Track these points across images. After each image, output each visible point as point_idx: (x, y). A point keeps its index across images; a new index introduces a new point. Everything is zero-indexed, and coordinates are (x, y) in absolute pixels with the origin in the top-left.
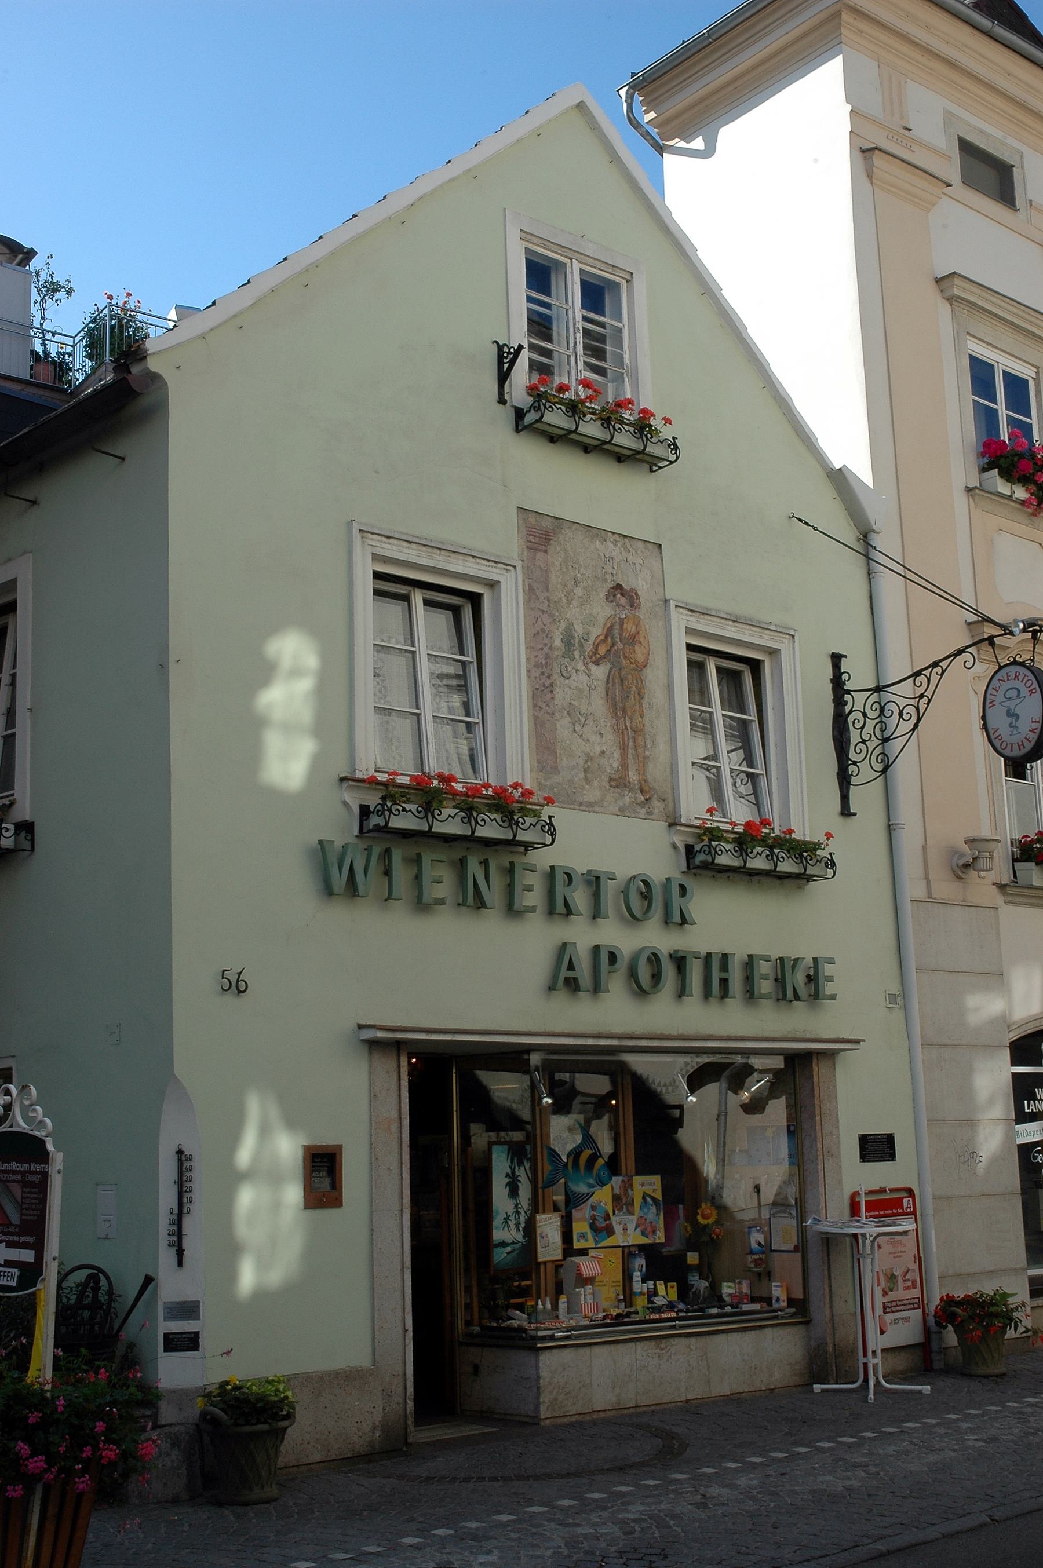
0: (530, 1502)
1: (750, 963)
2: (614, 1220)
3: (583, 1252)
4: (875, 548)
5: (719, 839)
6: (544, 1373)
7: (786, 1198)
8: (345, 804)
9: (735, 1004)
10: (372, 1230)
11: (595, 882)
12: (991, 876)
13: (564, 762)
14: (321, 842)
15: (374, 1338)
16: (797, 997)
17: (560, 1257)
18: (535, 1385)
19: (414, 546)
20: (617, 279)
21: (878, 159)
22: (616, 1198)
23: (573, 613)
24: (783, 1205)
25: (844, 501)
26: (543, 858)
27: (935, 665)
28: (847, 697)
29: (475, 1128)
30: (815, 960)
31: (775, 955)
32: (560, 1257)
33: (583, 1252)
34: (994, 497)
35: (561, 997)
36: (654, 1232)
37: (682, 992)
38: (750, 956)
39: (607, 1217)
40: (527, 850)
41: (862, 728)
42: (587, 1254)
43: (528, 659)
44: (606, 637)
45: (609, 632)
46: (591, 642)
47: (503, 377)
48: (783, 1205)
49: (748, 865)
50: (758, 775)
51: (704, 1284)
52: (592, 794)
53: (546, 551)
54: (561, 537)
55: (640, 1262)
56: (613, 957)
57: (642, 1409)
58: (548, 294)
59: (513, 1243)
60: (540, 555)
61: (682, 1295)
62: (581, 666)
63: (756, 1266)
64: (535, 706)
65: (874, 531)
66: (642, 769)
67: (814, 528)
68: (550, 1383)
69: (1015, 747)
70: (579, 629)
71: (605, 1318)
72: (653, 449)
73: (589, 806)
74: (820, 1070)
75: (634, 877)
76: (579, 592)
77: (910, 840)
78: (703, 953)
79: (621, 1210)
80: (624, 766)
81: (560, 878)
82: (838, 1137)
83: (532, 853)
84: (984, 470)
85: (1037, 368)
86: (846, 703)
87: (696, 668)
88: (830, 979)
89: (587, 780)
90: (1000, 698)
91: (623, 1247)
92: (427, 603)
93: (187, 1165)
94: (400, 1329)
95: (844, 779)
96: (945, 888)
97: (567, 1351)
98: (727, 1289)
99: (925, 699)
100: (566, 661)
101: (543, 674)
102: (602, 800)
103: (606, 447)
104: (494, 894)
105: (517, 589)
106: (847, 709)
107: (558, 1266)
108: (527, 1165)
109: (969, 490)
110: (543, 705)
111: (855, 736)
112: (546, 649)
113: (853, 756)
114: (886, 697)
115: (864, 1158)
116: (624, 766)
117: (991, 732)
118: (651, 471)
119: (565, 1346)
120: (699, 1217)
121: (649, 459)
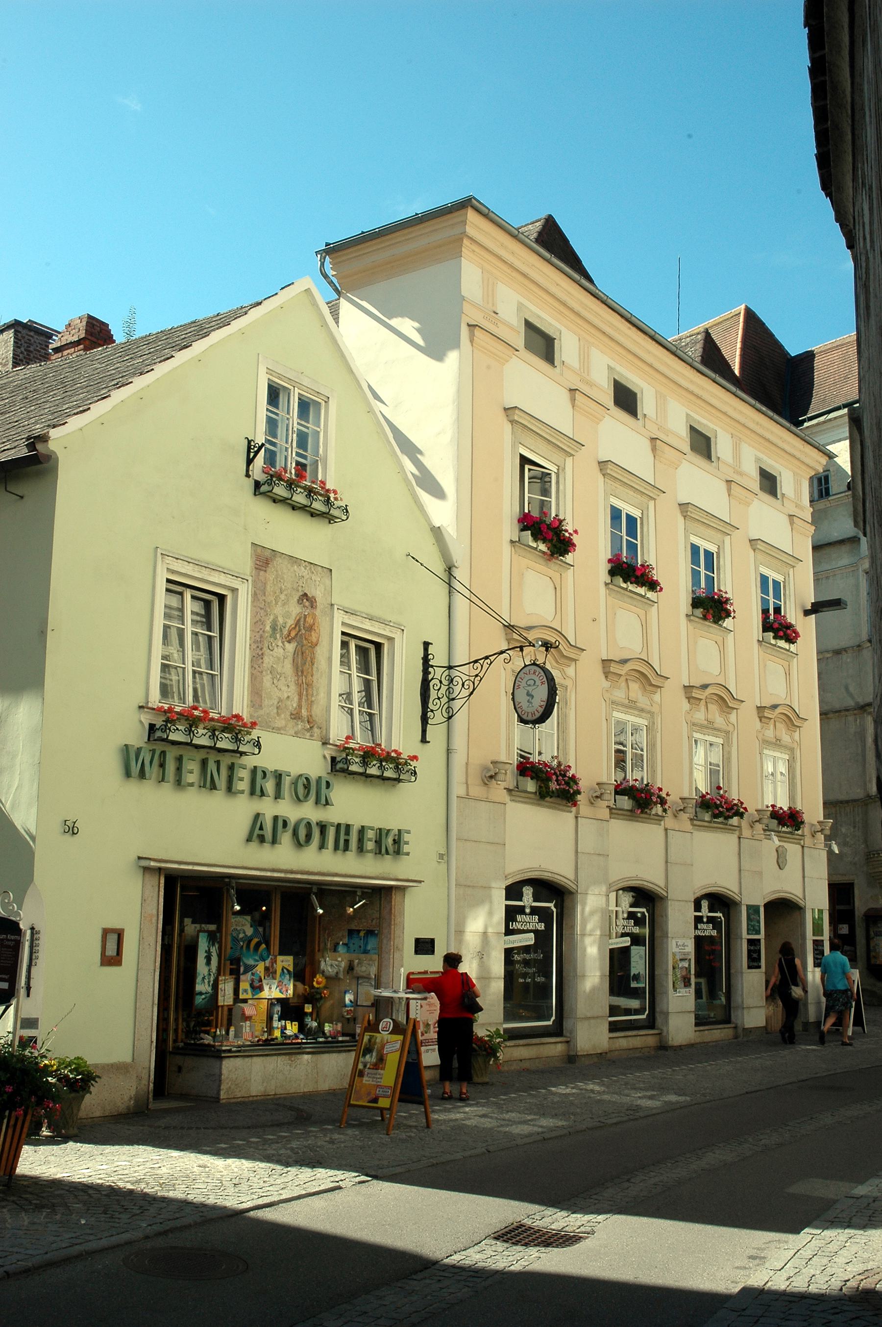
0: (234, 1139)
1: (362, 831)
2: (264, 982)
3: (245, 1001)
4: (455, 578)
5: (352, 755)
6: (225, 1071)
7: (370, 974)
8: (141, 722)
9: (351, 855)
10: (137, 981)
11: (279, 777)
12: (503, 785)
13: (266, 702)
14: (126, 745)
15: (134, 1046)
16: (387, 853)
17: (231, 1003)
18: (218, 1079)
19: (191, 564)
20: (319, 400)
21: (477, 332)
22: (267, 969)
23: (278, 610)
24: (367, 978)
25: (439, 546)
26: (250, 761)
27: (487, 658)
28: (430, 669)
29: (188, 921)
30: (399, 831)
31: (377, 825)
32: (231, 1003)
33: (245, 1001)
34: (526, 548)
35: (254, 845)
36: (287, 991)
37: (322, 846)
38: (363, 827)
39: (260, 980)
40: (241, 755)
41: (439, 690)
42: (247, 1002)
43: (250, 638)
44: (296, 626)
45: (297, 623)
46: (287, 629)
47: (250, 461)
48: (367, 978)
49: (367, 772)
50: (374, 714)
51: (315, 1024)
52: (280, 723)
53: (265, 571)
54: (275, 563)
55: (278, 1008)
56: (285, 824)
57: (278, 1096)
58: (277, 408)
59: (206, 993)
60: (262, 573)
61: (302, 1029)
62: (280, 644)
63: (347, 1014)
64: (252, 667)
65: (455, 566)
66: (309, 710)
67: (421, 564)
68: (227, 1078)
69: (530, 715)
70: (281, 620)
71: (258, 1041)
72: (334, 512)
73: (278, 730)
74: (396, 897)
75: (301, 775)
76: (283, 597)
77: (459, 760)
78: (336, 823)
79: (269, 976)
80: (300, 706)
81: (259, 774)
82: (403, 939)
83: (244, 758)
84: (522, 530)
85: (558, 466)
86: (430, 673)
87: (345, 645)
88: (407, 843)
89: (278, 714)
90: (523, 684)
91: (268, 999)
92: (193, 597)
93: (36, 936)
94: (149, 1041)
95: (425, 720)
96: (477, 790)
97: (238, 1059)
98: (327, 1028)
99: (479, 678)
100: (272, 639)
101: (258, 647)
102: (286, 726)
103: (307, 508)
104: (222, 782)
105: (248, 594)
106: (430, 677)
107: (230, 1010)
108: (217, 946)
109: (512, 542)
110: (257, 667)
111: (433, 694)
112: (261, 632)
113: (431, 706)
114: (454, 673)
115: (417, 952)
116: (300, 706)
117: (516, 704)
118: (330, 523)
119: (237, 1056)
120: (315, 983)
121: (330, 517)
